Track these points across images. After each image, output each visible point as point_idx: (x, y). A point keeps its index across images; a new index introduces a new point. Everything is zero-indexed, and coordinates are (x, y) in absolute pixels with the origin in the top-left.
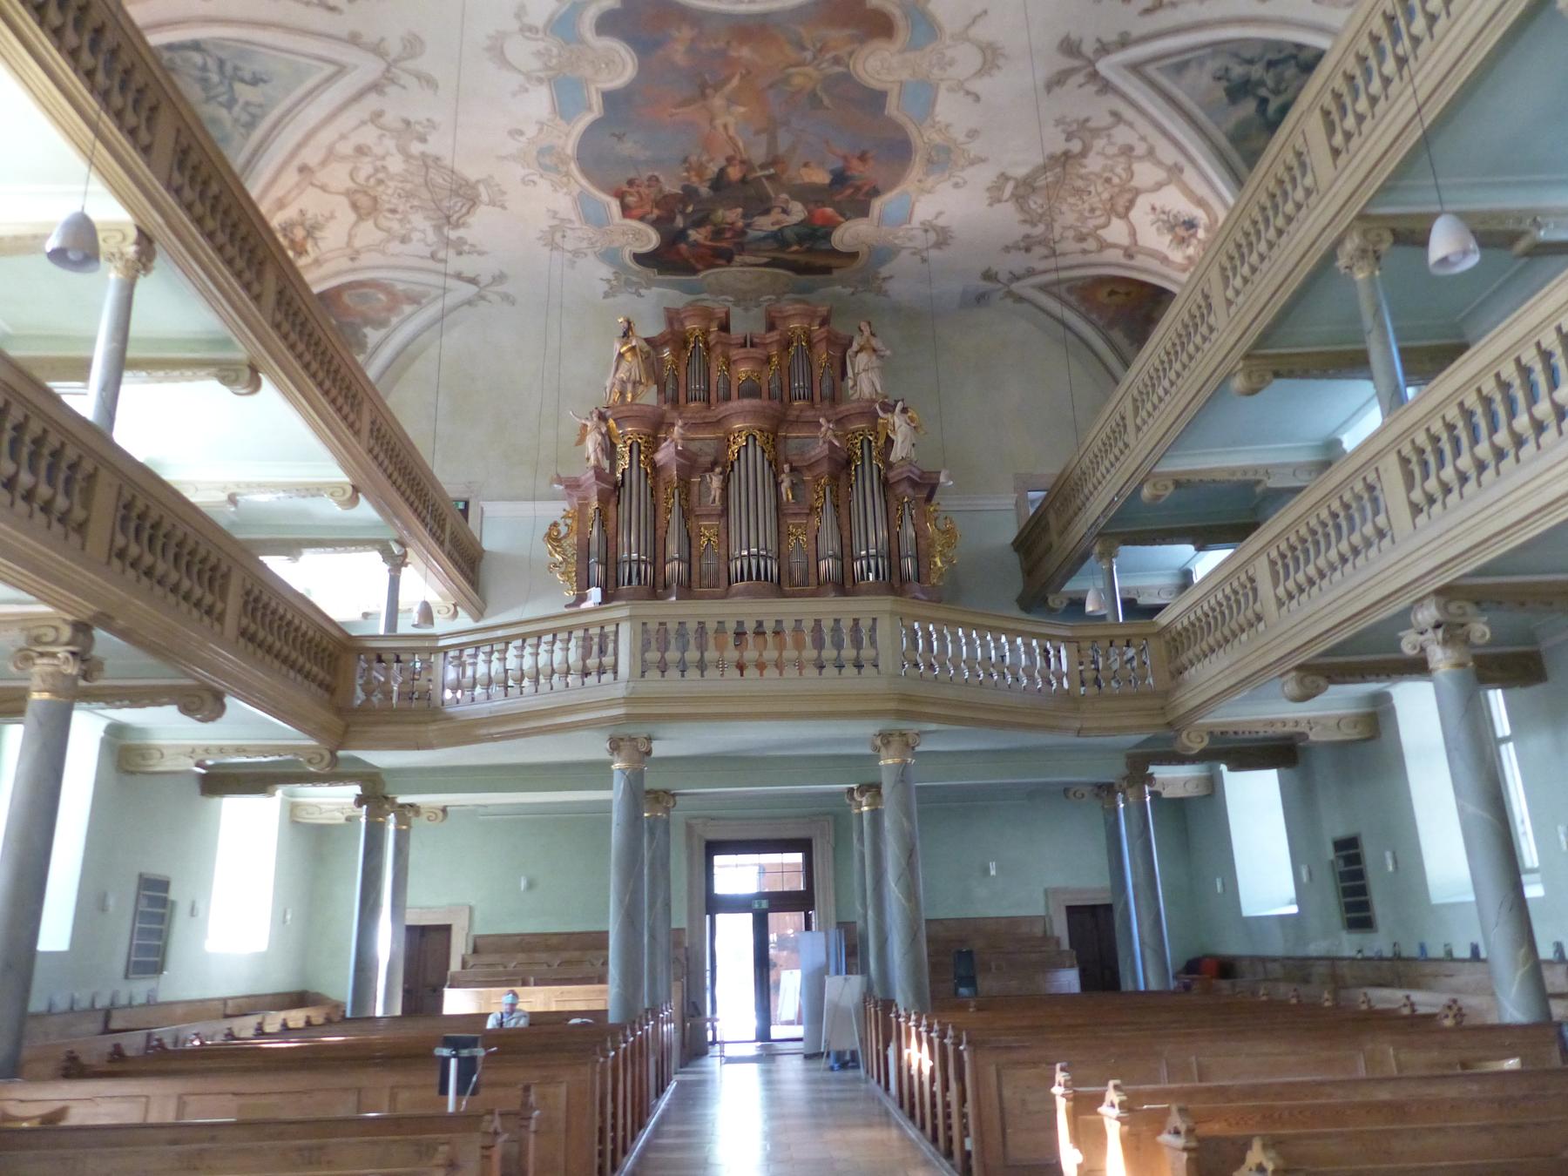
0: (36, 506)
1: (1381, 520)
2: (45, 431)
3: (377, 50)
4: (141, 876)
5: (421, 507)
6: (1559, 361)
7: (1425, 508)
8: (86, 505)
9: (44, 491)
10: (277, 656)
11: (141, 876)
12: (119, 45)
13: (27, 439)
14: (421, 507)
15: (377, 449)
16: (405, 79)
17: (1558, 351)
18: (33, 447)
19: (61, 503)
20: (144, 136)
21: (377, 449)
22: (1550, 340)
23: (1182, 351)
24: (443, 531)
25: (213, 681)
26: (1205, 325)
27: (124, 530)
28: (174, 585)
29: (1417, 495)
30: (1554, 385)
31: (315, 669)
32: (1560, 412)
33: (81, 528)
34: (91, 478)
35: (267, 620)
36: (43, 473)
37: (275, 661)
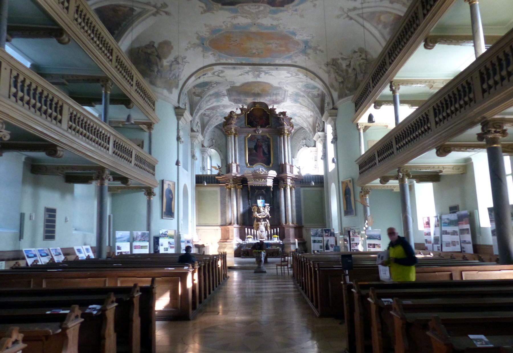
0: (47, 115)
1: (429, 125)
2: (31, 83)
3: (155, 6)
4: (45, 208)
5: (143, 95)
6: (511, 58)
7: (443, 120)
8: (61, 114)
9: (38, 105)
10: (118, 156)
11: (45, 208)
12: (79, 5)
13: (54, 103)
14: (143, 95)
15: (119, 67)
16: (161, 13)
17: (510, 54)
18: (74, 117)
19: (38, 105)
20: (66, 4)
21: (119, 67)
22: (508, 50)
23: (404, 37)
24: (132, 80)
25: (40, 135)
26: (405, 38)
27: (16, 86)
28: (33, 105)
29: (437, 119)
30: (508, 65)
31: (125, 156)
32: (509, 74)
33: (60, 121)
34: (61, 107)
35: (93, 131)
36: (58, 112)
37: (99, 146)
